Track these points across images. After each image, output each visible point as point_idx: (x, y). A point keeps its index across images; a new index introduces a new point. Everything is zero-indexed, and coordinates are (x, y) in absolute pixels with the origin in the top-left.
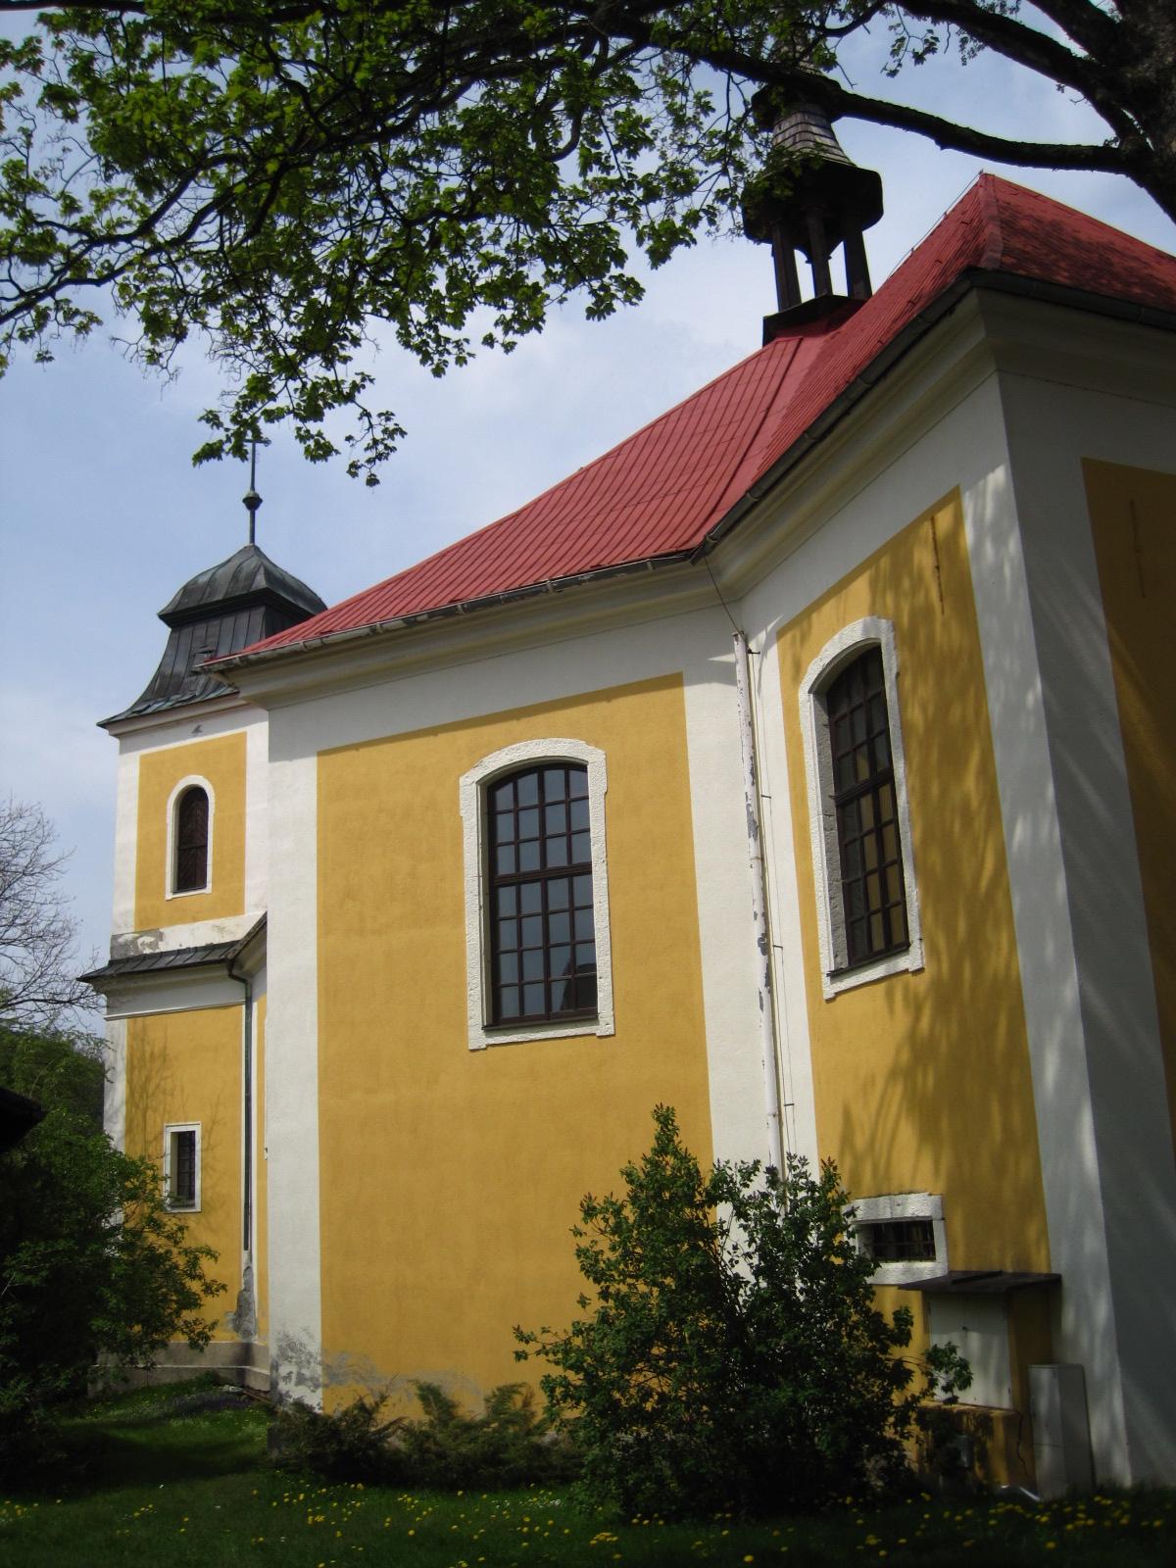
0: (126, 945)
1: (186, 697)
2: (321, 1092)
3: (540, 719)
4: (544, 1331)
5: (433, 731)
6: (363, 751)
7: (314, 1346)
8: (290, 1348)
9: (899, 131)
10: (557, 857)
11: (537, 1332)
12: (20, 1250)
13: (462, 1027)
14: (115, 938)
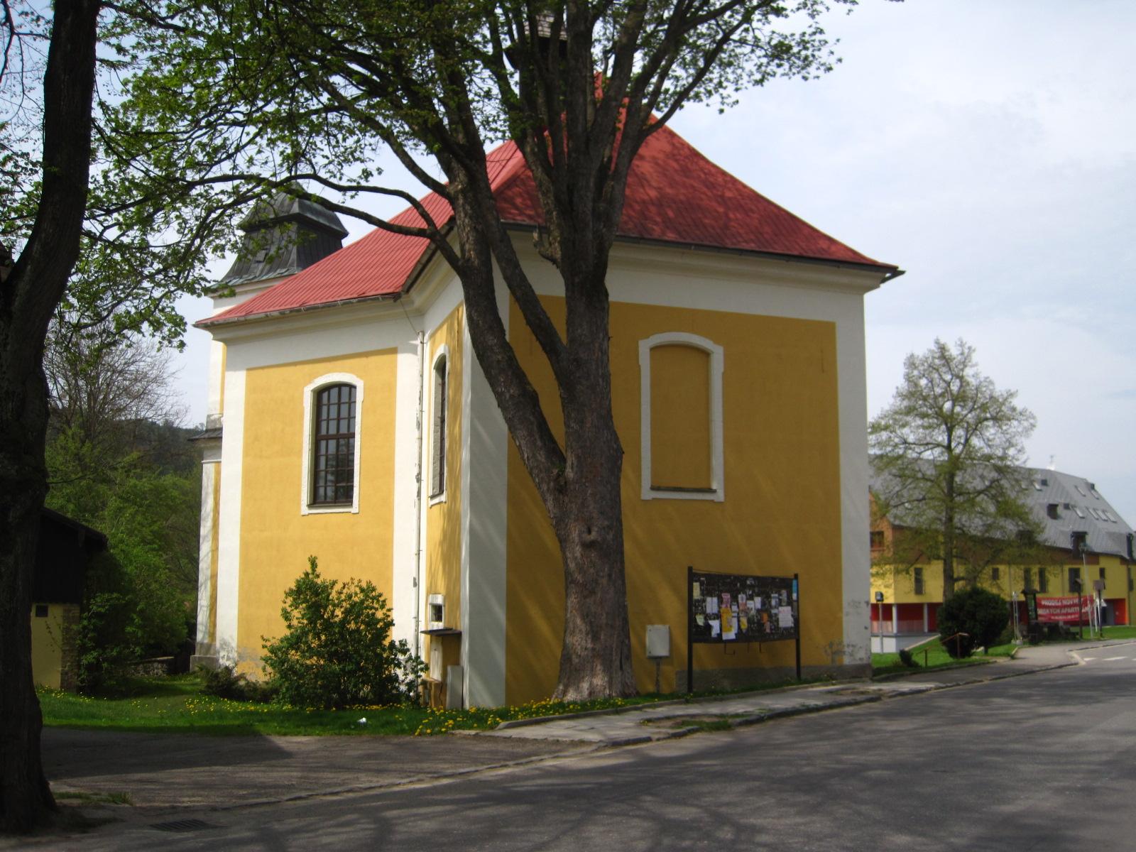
0: (214, 421)
1: (251, 277)
2: (241, 530)
3: (339, 363)
4: (274, 638)
5: (295, 364)
6: (266, 370)
7: (234, 644)
8: (225, 644)
9: (357, 219)
10: (343, 430)
11: (271, 639)
12: (97, 597)
13: (299, 504)
14: (209, 416)
